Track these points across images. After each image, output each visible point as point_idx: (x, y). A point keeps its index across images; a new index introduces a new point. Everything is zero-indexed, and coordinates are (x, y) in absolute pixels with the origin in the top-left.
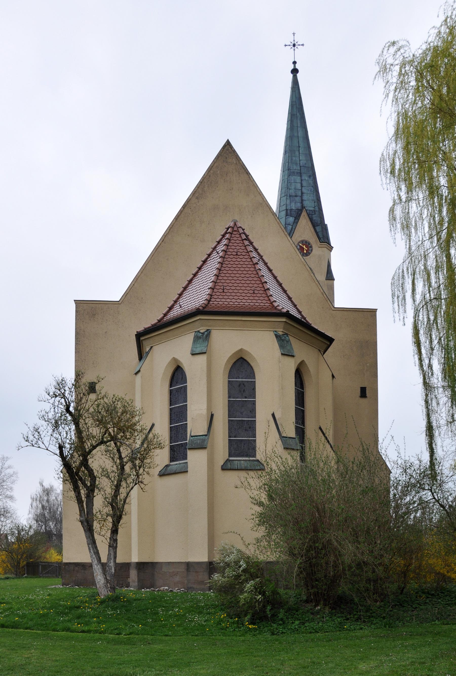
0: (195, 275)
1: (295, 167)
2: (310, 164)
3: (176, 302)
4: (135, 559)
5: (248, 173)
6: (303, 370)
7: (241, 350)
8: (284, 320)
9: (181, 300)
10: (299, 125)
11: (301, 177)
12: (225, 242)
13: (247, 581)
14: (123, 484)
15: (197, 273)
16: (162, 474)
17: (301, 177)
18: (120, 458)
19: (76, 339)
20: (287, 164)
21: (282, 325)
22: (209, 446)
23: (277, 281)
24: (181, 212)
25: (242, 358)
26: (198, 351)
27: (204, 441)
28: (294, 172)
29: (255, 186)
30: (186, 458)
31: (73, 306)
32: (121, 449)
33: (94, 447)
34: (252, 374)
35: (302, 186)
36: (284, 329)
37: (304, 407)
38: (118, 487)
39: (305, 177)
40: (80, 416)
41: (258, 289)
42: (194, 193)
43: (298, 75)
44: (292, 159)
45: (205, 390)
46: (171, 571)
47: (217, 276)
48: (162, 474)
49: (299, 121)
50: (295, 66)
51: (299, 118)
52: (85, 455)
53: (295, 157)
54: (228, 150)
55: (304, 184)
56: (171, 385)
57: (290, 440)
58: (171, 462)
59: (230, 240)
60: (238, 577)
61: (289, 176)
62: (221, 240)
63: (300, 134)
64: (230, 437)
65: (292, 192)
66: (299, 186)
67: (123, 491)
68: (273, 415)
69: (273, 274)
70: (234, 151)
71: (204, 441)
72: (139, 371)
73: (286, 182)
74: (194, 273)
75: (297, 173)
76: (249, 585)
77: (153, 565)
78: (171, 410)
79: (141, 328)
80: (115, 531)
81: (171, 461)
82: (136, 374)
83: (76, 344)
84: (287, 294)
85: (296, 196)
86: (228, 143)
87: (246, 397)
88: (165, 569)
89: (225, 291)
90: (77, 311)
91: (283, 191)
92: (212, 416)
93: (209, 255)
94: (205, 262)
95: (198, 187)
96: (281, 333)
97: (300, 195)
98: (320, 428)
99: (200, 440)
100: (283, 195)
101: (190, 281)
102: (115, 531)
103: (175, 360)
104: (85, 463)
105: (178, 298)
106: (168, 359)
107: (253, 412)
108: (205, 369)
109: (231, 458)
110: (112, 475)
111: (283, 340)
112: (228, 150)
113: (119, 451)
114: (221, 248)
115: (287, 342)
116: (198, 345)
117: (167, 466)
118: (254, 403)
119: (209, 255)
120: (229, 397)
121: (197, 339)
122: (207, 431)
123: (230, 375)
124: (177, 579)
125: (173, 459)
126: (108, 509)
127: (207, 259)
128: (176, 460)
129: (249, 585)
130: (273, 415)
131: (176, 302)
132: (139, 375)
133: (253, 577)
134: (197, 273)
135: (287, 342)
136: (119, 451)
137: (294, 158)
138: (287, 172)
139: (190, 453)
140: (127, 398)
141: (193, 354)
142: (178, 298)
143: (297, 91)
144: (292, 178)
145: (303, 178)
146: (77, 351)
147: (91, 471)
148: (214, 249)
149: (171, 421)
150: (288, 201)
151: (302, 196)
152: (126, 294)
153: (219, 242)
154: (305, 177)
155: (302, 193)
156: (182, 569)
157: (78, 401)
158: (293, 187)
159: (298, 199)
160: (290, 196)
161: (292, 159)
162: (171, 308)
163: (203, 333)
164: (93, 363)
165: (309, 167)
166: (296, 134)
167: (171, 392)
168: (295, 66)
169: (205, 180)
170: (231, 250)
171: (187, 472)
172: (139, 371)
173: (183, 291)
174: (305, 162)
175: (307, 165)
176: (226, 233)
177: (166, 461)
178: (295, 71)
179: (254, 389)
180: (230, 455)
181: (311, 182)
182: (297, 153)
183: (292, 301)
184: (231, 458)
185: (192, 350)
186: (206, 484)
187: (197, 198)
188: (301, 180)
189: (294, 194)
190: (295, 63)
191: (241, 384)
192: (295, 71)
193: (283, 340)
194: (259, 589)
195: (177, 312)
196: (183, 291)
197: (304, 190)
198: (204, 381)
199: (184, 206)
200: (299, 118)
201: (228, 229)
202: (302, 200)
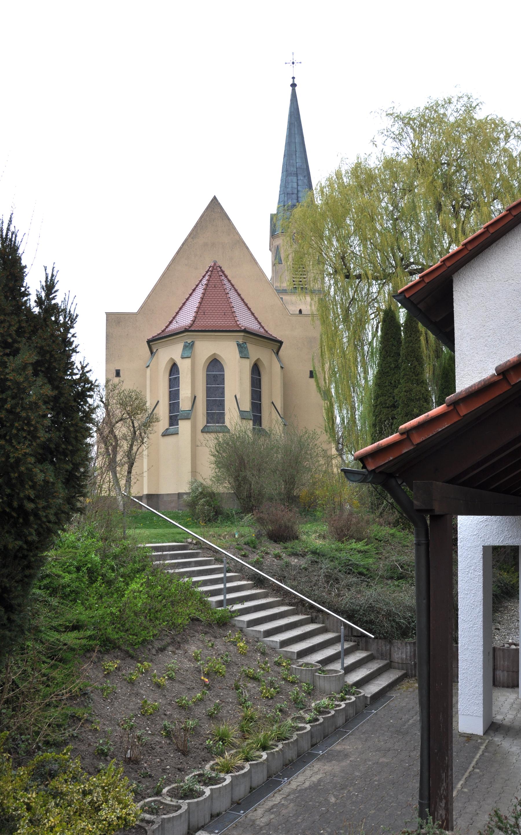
0: (187, 300)
1: (292, 169)
2: (305, 166)
3: (174, 318)
4: (146, 492)
5: (229, 219)
6: (259, 364)
7: (215, 354)
8: (243, 334)
9: (177, 318)
10: (296, 132)
11: (297, 177)
12: (207, 278)
13: (201, 499)
14: (135, 443)
15: (189, 298)
16: (164, 435)
17: (297, 177)
18: (134, 427)
19: (107, 339)
20: (285, 166)
21: (242, 337)
22: (192, 417)
23: (244, 302)
24: (181, 248)
25: (215, 359)
26: (185, 356)
27: (189, 414)
28: (291, 173)
29: (234, 228)
30: (178, 425)
31: (104, 317)
32: (135, 421)
33: (117, 422)
34: (222, 369)
35: (298, 185)
36: (243, 339)
37: (260, 389)
38: (132, 446)
39: (301, 177)
40: (109, 405)
41: (228, 311)
42: (190, 235)
43: (296, 88)
44: (289, 162)
45: (190, 381)
46: (169, 499)
47: (200, 303)
48: (164, 435)
49: (296, 129)
50: (294, 81)
51: (296, 126)
52: (112, 427)
53: (292, 160)
54: (215, 203)
55: (300, 183)
56: (170, 375)
57: (246, 413)
58: (170, 426)
59: (212, 272)
60: (197, 497)
61: (287, 177)
62: (205, 275)
63: (297, 140)
64: (207, 410)
65: (289, 190)
66: (295, 185)
67: (135, 448)
68: (236, 396)
69: (241, 298)
70: (219, 204)
71: (189, 414)
72: (149, 366)
73: (284, 182)
74: (190, 293)
75: (294, 174)
76: (202, 501)
77: (157, 496)
78: (170, 392)
79: (150, 337)
80: (129, 472)
81: (170, 426)
82: (147, 367)
83: (106, 343)
84: (251, 311)
85: (292, 194)
86: (215, 198)
87: (218, 385)
88: (165, 499)
89: (205, 313)
90: (107, 320)
91: (282, 189)
92: (195, 397)
93: (197, 286)
94: (194, 290)
95: (193, 230)
96: (241, 342)
97: (296, 192)
98: (273, 403)
99: (186, 413)
100: (282, 193)
101: (184, 304)
102: (129, 472)
103: (172, 359)
104: (112, 432)
105: (176, 315)
106: (168, 359)
107: (223, 394)
108: (190, 368)
109: (208, 425)
110: (128, 438)
111: (242, 347)
112: (215, 203)
113: (133, 423)
114: (204, 282)
115: (245, 348)
116: (186, 352)
117: (167, 429)
118: (223, 388)
119: (197, 286)
120: (207, 384)
121: (185, 347)
122: (191, 407)
123: (208, 370)
124: (173, 505)
125: (171, 424)
126: (126, 459)
127: (195, 288)
128: (173, 426)
129: (202, 501)
130: (236, 396)
131: (174, 318)
132: (149, 368)
133: (205, 496)
134: (189, 298)
135: (245, 348)
136: (133, 423)
137: (291, 161)
138: (285, 173)
139: (180, 422)
140: (138, 390)
141: (182, 358)
142: (176, 315)
143: (295, 103)
144: (290, 178)
145: (299, 178)
146: (107, 348)
147: (115, 437)
148: (201, 281)
149: (170, 399)
150: (286, 198)
151: (297, 194)
152: (142, 308)
153: (204, 277)
154: (301, 177)
155: (298, 191)
156: (176, 498)
157: (108, 395)
158: (290, 186)
159: (294, 196)
160: (287, 194)
161: (289, 162)
162: (171, 322)
163: (189, 344)
164: (118, 356)
165: (304, 169)
166: (293, 141)
167: (170, 380)
168: (294, 81)
169: (198, 225)
170: (211, 284)
171: (178, 434)
172: (149, 366)
173: (179, 311)
174: (301, 164)
175: (302, 167)
176: (208, 270)
177: (167, 426)
178: (294, 85)
179: (224, 379)
180: (207, 422)
181: (306, 181)
182: (294, 157)
183: (254, 316)
184: (208, 425)
185: (182, 355)
186: (190, 442)
187: (192, 238)
188: (297, 180)
189: (291, 192)
190: (293, 78)
191: (215, 376)
192: (294, 85)
193: (242, 347)
194: (208, 503)
195: (174, 326)
196: (179, 311)
197: (300, 189)
198: (189, 375)
199: (183, 244)
200: (296, 126)
201: (210, 267)
202: (298, 197)
